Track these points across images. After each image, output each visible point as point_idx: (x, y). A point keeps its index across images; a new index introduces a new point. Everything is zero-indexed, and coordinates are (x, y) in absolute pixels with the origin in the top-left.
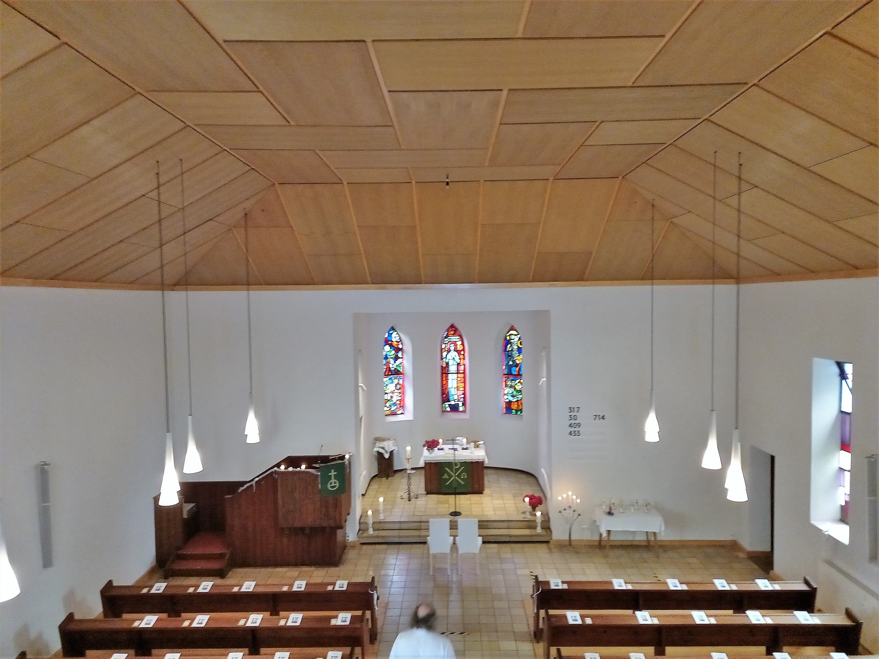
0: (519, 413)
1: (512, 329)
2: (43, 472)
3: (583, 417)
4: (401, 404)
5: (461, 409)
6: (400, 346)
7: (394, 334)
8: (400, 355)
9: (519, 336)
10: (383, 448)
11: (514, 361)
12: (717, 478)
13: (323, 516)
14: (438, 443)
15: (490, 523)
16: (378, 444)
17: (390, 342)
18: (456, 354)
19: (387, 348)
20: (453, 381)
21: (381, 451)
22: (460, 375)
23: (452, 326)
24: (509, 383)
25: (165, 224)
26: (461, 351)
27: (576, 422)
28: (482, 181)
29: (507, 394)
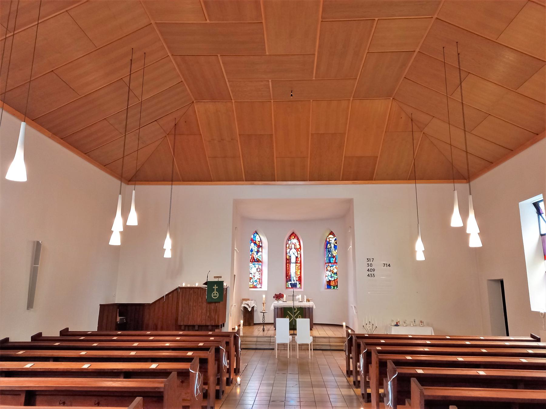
2: (38, 246)
3: (377, 265)
4: (260, 282)
6: (261, 245)
7: (257, 237)
8: (260, 249)
9: (335, 238)
10: (248, 305)
11: (332, 254)
12: (462, 232)
15: (317, 339)
16: (244, 302)
17: (254, 241)
19: (252, 244)
20: (293, 268)
21: (247, 307)
23: (293, 233)
25: (125, 158)
26: (298, 249)
28: (311, 101)
29: (326, 276)
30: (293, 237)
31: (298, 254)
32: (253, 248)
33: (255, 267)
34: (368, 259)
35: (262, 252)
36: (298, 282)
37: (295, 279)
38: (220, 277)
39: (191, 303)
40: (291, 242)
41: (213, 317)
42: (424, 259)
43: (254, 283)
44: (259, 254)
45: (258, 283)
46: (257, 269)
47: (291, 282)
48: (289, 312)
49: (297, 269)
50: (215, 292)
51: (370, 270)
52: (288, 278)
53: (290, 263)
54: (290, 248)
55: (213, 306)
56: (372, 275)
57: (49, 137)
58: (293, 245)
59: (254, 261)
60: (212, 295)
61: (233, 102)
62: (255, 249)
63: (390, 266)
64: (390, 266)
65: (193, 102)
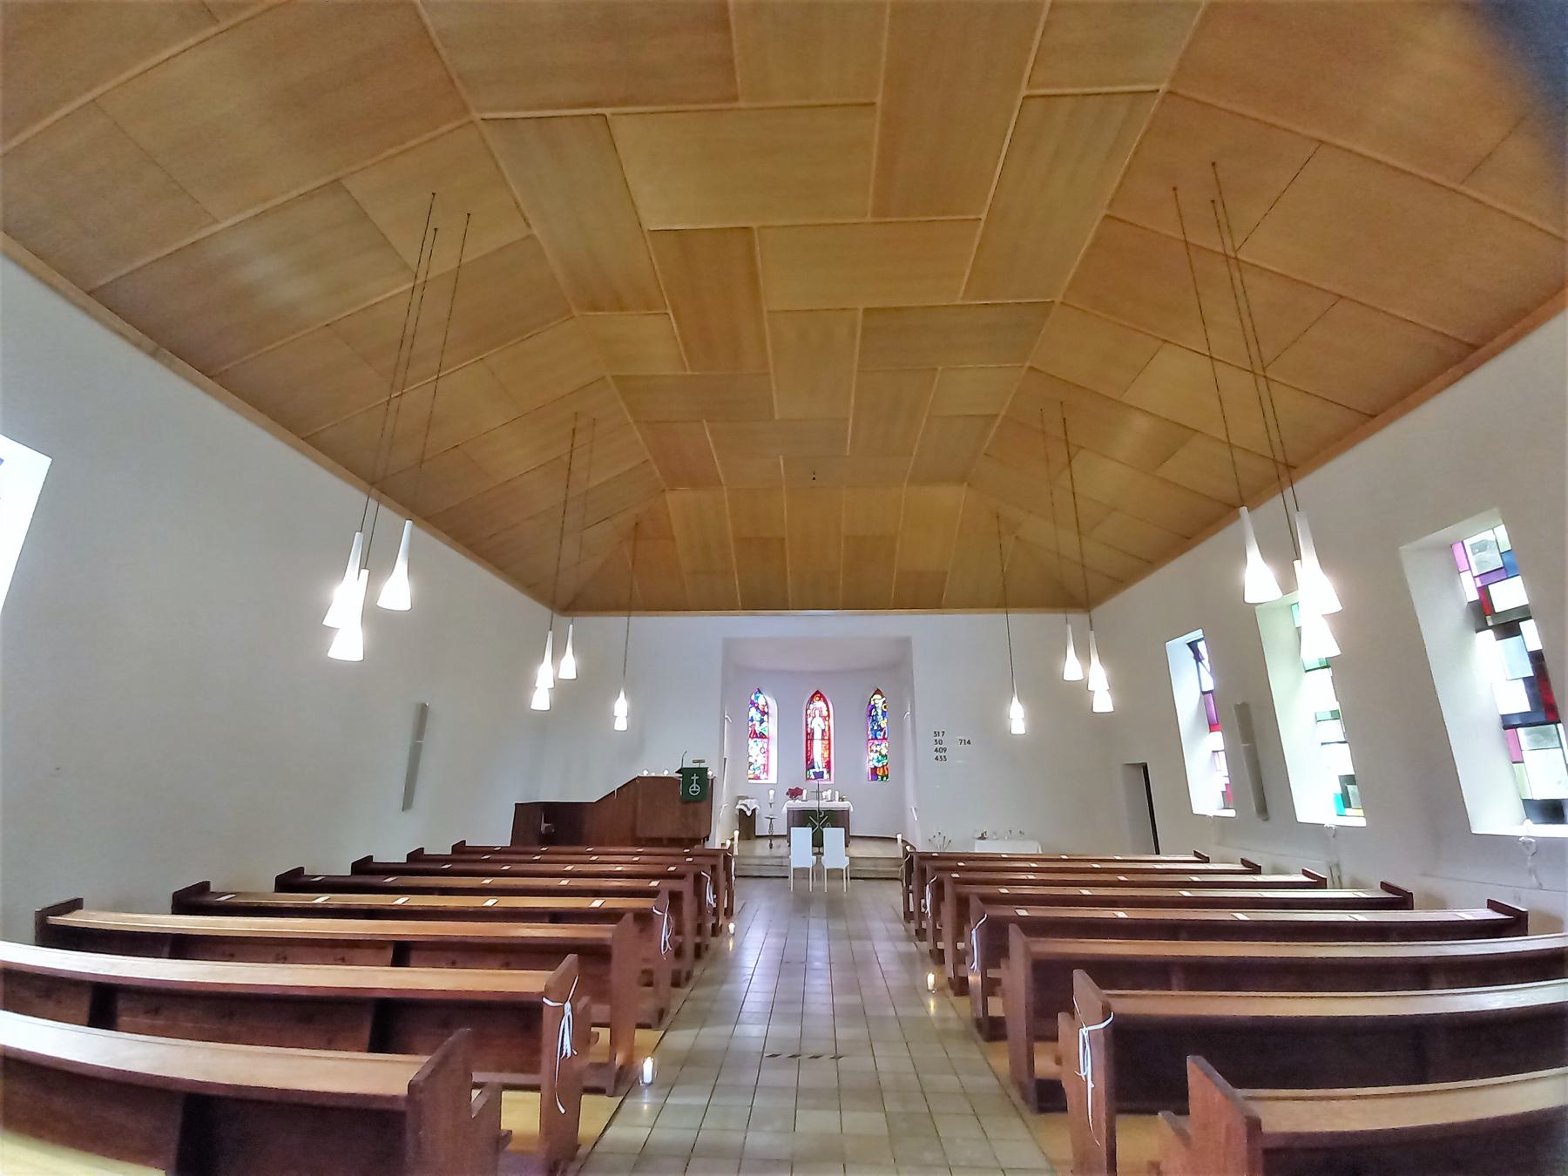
0: (885, 778)
1: (878, 692)
6: (766, 710)
10: (746, 806)
11: (879, 726)
14: (801, 794)
16: (740, 802)
18: (821, 719)
19: (753, 709)
21: (743, 807)
22: (824, 742)
23: (817, 692)
24: (874, 748)
27: (941, 746)
30: (818, 698)
37: (820, 765)
44: (764, 724)
53: (812, 740)
62: (757, 716)
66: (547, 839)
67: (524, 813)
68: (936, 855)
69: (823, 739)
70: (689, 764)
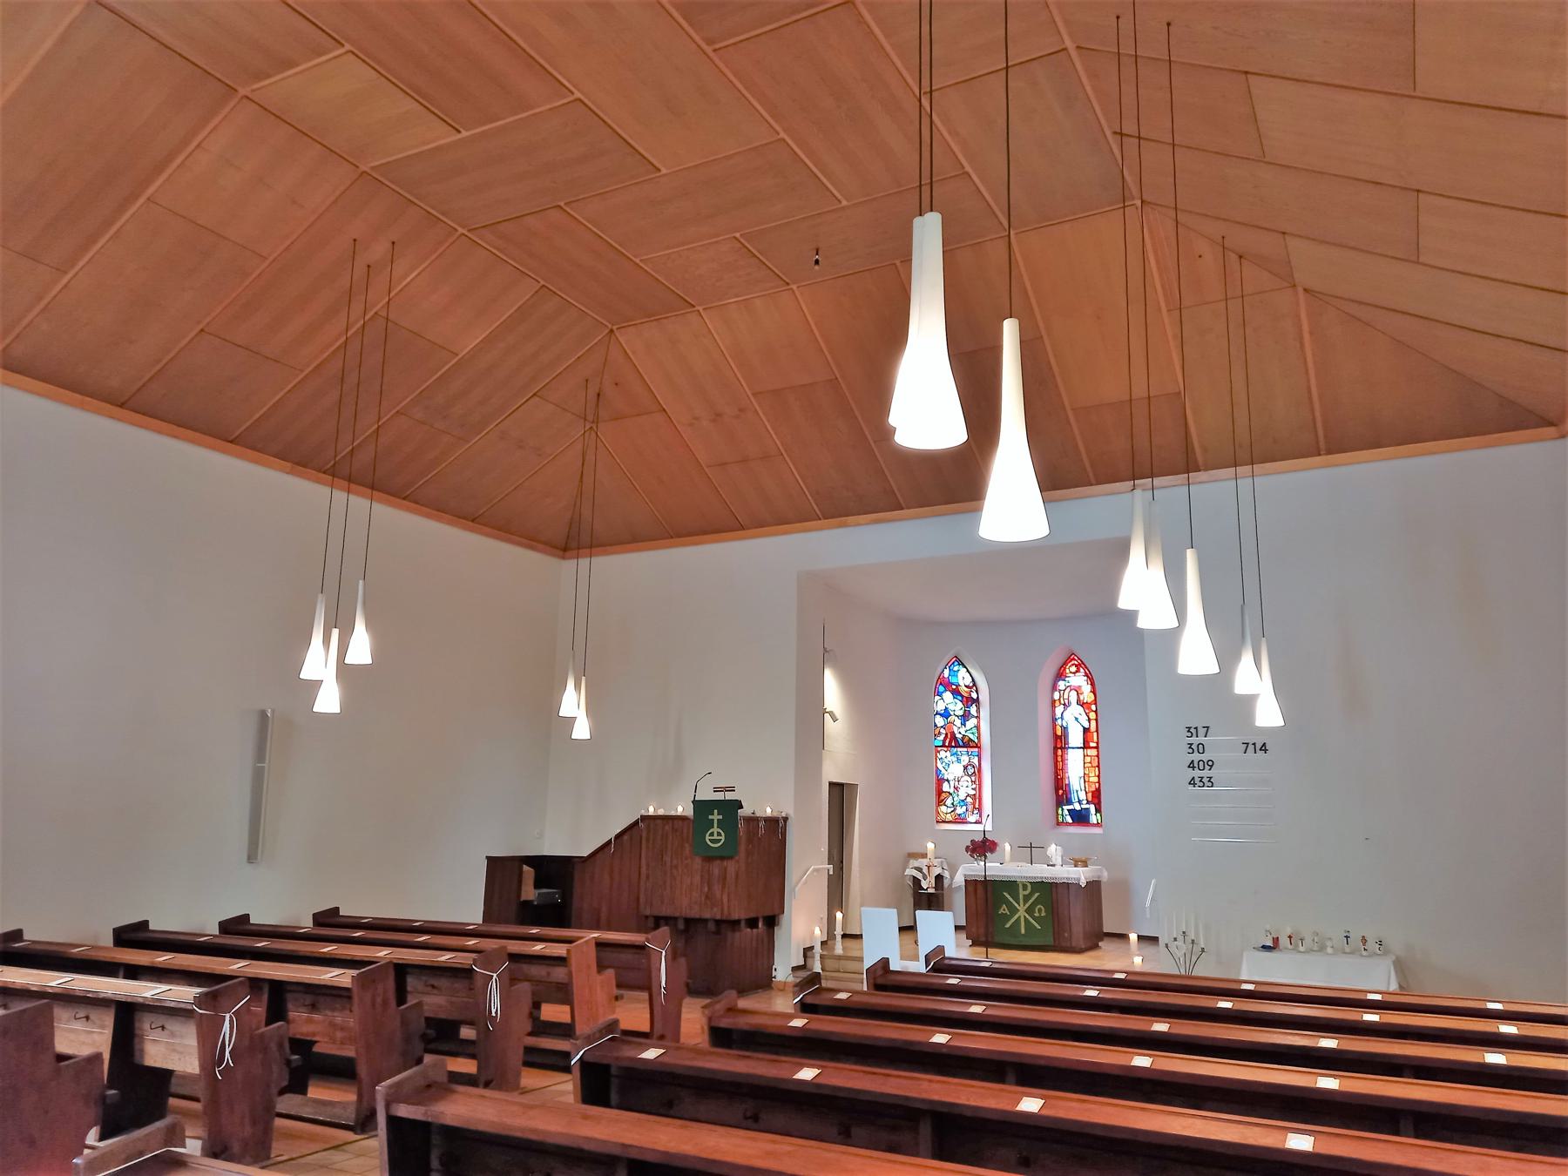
5: (1094, 819)
6: (974, 695)
10: (919, 869)
13: (703, 899)
17: (954, 687)
19: (948, 696)
21: (919, 876)
26: (1090, 704)
27: (1202, 757)
30: (1074, 669)
31: (1089, 720)
32: (951, 707)
33: (959, 761)
34: (1190, 728)
35: (978, 717)
36: (1092, 808)
37: (1082, 796)
38: (732, 789)
39: (667, 859)
40: (1068, 684)
41: (718, 894)
42: (337, 710)
43: (958, 808)
44: (971, 723)
45: (970, 807)
46: (965, 768)
47: (1070, 807)
48: (1008, 896)
49: (1090, 765)
50: (715, 830)
51: (1196, 765)
52: (1063, 794)
53: (1065, 748)
54: (1064, 704)
55: (716, 869)
56: (1205, 780)
57: (288, 473)
58: (1074, 694)
59: (953, 744)
60: (708, 838)
61: (701, 311)
62: (957, 707)
63: (1266, 751)
64: (1266, 751)
65: (612, 331)
66: (532, 914)
67: (500, 870)
68: (1122, 976)
69: (1086, 746)
70: (706, 794)
